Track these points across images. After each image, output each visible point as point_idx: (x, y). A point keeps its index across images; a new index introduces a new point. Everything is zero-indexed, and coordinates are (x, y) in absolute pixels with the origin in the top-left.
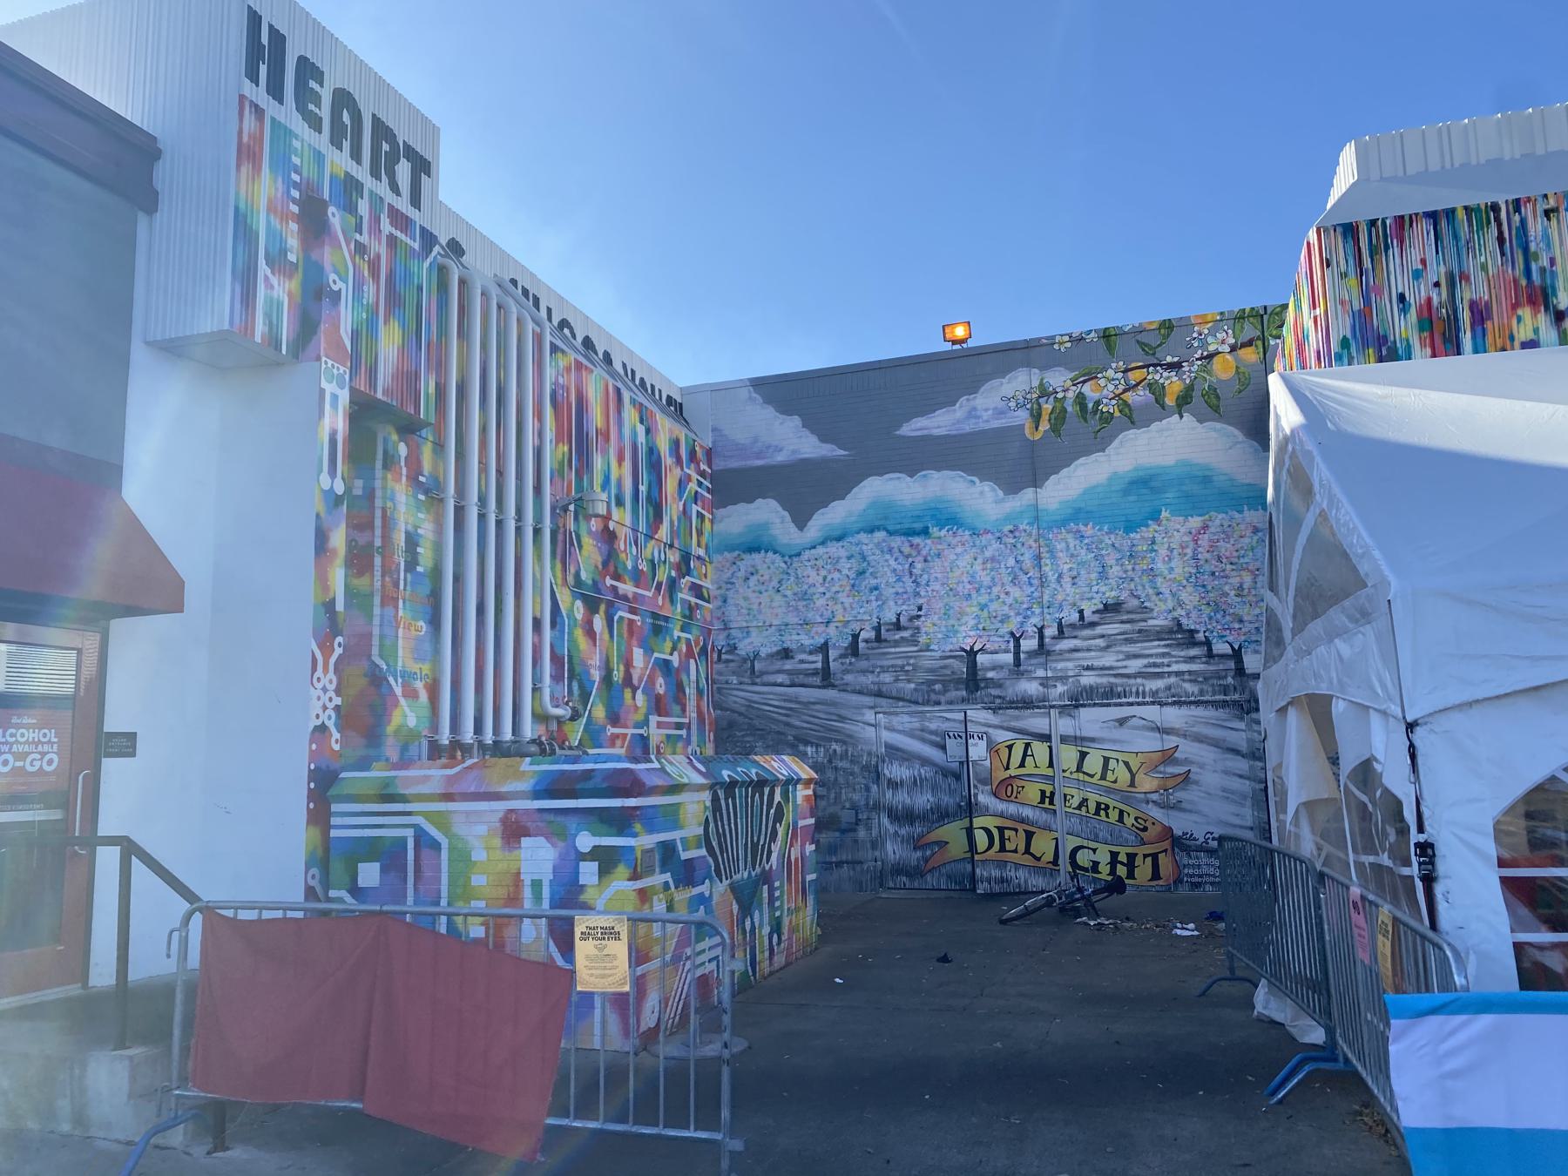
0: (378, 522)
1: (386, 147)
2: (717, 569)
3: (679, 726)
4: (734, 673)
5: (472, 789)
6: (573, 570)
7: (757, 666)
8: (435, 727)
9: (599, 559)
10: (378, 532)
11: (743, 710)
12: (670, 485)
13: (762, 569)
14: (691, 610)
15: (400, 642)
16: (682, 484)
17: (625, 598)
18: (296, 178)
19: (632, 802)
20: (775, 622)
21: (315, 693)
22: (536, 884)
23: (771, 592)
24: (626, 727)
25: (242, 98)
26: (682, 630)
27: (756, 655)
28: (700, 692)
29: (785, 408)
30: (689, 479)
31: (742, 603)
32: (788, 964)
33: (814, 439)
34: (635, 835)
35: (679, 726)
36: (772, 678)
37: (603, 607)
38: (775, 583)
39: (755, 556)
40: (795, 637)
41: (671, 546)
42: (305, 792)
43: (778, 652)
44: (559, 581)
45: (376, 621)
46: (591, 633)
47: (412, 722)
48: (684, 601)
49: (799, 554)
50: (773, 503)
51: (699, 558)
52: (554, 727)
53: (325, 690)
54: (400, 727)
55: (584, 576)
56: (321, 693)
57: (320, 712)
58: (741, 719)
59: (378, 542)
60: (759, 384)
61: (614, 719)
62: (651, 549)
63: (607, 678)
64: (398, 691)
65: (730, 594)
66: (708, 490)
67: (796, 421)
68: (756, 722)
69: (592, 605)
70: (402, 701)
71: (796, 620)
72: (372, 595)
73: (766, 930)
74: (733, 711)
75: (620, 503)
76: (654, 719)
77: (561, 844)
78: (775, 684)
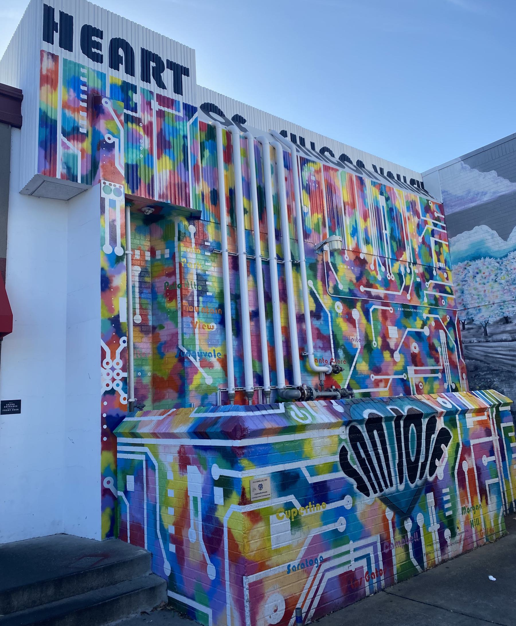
0: (178, 271)
1: (152, 64)
2: (456, 274)
3: (433, 371)
4: (474, 336)
5: (163, 431)
6: (331, 284)
7: (488, 330)
8: (226, 383)
9: (353, 277)
10: (178, 276)
11: (482, 358)
12: (410, 228)
13: (483, 269)
14: (436, 302)
15: (197, 336)
16: (419, 227)
17: (378, 297)
18: (83, 88)
19: (237, 443)
20: (497, 301)
22: (195, 499)
23: (491, 283)
24: (388, 375)
25: (42, 52)
26: (430, 312)
27: (487, 323)
28: (450, 350)
29: (485, 168)
30: (426, 223)
31: (474, 292)
32: (466, 551)
33: (507, 182)
34: (241, 469)
35: (433, 371)
36: (499, 337)
37: (359, 305)
38: (493, 277)
39: (478, 262)
40: (511, 309)
41: (415, 263)
42: (100, 431)
43: (501, 320)
45: (180, 325)
46: (351, 320)
47: (209, 381)
48: (429, 296)
49: (506, 256)
50: (485, 227)
51: (440, 268)
52: (323, 378)
53: (113, 369)
54: (199, 386)
55: (341, 287)
56: (110, 372)
57: (110, 382)
58: (482, 365)
59: (178, 282)
60: (466, 158)
61: (377, 371)
62: (396, 267)
63: (368, 345)
64: (197, 364)
65: (465, 288)
66: (443, 228)
67: (494, 173)
68: (492, 365)
69: (350, 303)
70: (201, 370)
71: (510, 298)
72: (177, 311)
73: (435, 527)
74: (477, 360)
75: (367, 242)
76: (411, 369)
77: (205, 472)
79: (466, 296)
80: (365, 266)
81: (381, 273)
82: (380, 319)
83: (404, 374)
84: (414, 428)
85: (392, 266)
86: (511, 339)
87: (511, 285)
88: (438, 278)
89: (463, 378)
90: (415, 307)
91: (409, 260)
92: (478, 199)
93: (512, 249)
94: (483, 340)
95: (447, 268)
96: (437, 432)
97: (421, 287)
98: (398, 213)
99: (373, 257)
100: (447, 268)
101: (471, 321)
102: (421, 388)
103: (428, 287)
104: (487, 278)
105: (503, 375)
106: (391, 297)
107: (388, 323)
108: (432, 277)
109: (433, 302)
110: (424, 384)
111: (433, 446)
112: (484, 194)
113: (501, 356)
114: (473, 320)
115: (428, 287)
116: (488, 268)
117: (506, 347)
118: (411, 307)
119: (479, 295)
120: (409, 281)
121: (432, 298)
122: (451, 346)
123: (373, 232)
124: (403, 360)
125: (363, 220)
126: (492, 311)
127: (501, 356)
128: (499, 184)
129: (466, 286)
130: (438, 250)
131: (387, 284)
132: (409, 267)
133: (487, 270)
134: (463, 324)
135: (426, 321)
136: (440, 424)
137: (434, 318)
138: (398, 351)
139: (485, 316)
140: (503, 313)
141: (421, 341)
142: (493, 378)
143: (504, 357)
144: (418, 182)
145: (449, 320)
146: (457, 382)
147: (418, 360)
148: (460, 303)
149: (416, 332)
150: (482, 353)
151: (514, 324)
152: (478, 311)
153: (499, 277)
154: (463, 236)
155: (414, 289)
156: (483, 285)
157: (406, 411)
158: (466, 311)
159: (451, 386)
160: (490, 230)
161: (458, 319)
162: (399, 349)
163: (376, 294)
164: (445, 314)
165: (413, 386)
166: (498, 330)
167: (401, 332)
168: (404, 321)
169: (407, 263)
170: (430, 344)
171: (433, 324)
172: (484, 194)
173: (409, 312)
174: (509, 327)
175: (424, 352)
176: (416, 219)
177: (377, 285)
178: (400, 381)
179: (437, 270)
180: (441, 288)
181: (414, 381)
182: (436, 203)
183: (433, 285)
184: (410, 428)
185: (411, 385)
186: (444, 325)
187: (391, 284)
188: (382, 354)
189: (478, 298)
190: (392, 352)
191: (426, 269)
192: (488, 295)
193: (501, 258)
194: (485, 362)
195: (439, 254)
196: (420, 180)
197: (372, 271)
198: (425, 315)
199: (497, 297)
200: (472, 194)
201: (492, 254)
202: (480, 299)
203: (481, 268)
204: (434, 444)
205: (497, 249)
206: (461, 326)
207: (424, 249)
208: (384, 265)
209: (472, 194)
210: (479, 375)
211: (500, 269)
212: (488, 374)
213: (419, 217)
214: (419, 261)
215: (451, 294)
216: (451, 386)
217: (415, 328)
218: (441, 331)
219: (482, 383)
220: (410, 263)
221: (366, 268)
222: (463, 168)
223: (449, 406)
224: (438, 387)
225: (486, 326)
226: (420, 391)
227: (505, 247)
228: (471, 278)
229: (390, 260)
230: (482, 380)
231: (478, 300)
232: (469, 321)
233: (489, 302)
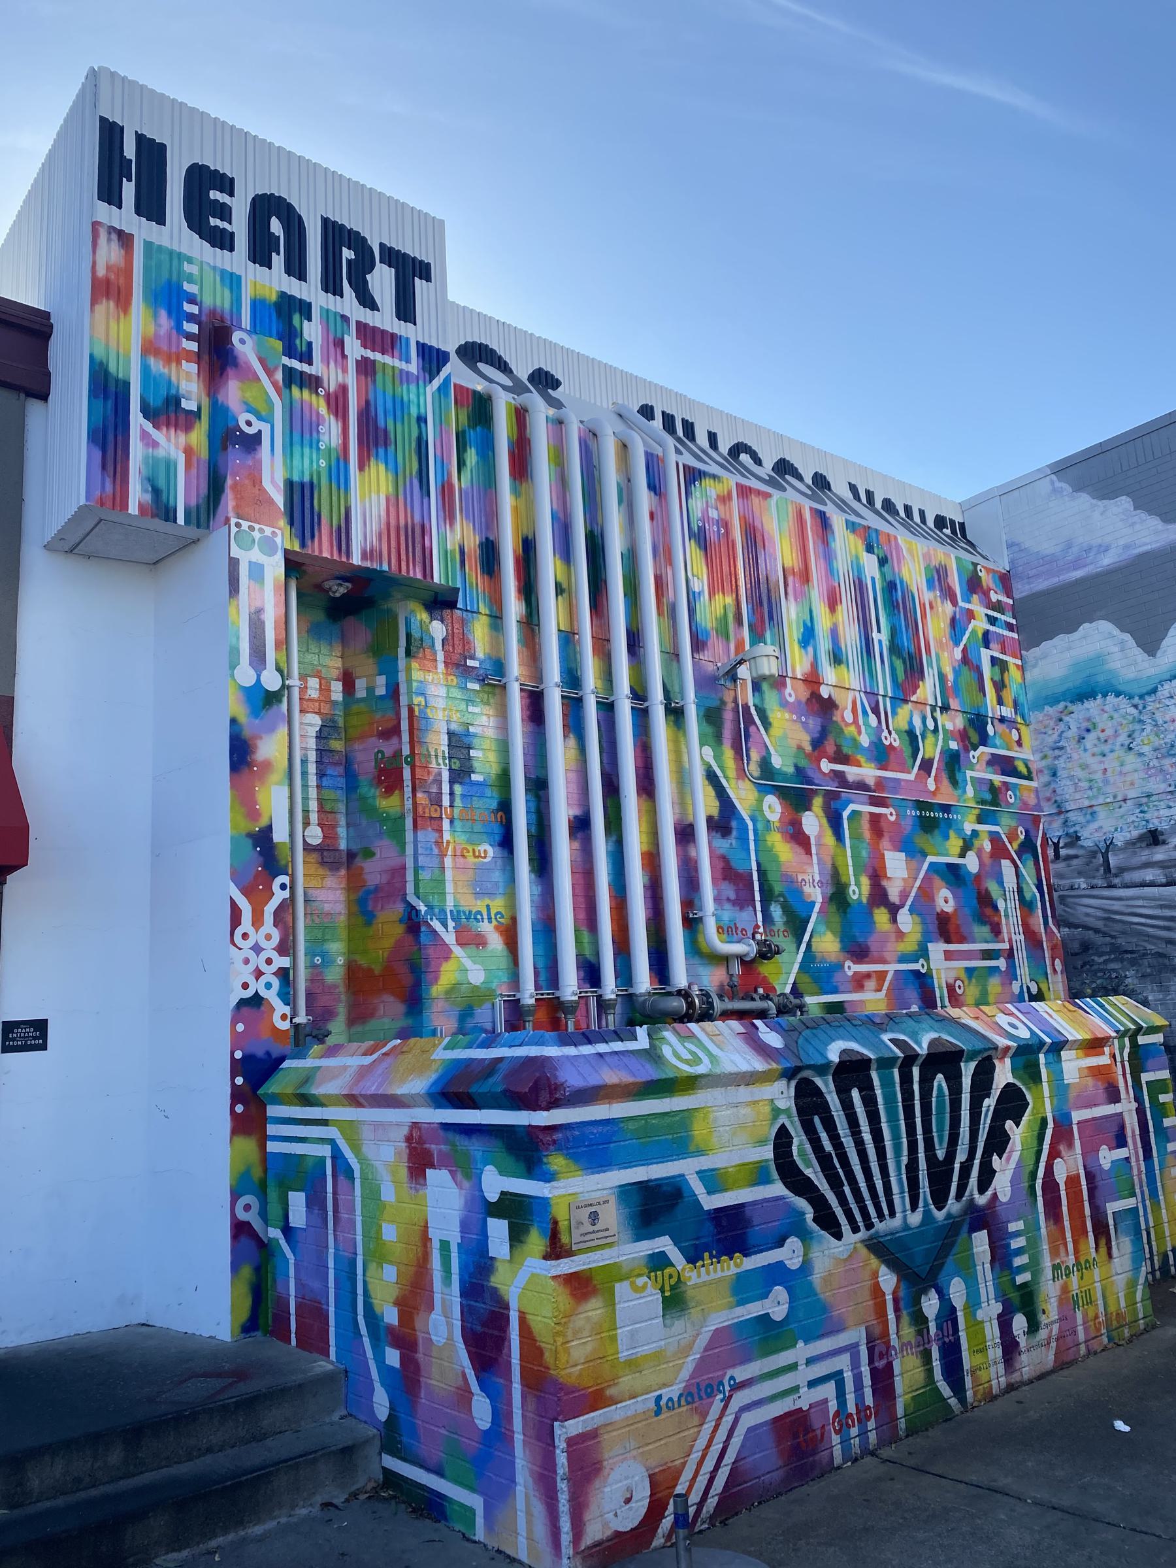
0: (405, 725)
1: (347, 254)
2: (1038, 732)
3: (988, 955)
4: (1080, 874)
5: (372, 1090)
6: (755, 756)
8: (515, 981)
9: (805, 740)
10: (405, 737)
11: (1100, 924)
12: (935, 627)
13: (1102, 721)
14: (993, 796)
15: (449, 874)
16: (956, 626)
17: (861, 786)
18: (190, 308)
19: (541, 1118)
21: (237, 956)
23: (1120, 752)
25: (96, 225)
26: (980, 820)
27: (1110, 845)
28: (1026, 906)
29: (1105, 490)
30: (970, 615)
31: (1079, 773)
32: (1062, 1365)
33: (1154, 522)
34: (549, 1177)
35: (988, 955)
36: (1137, 876)
37: (818, 802)
38: (1123, 738)
39: (1089, 704)
40: (1164, 812)
41: (945, 708)
42: (228, 1090)
43: (1141, 838)
44: (732, 773)
45: (409, 850)
46: (799, 838)
47: (477, 977)
48: (977, 782)
49: (1154, 691)
50: (1105, 626)
51: (1002, 720)
52: (737, 969)
53: (257, 949)
54: (454, 988)
55: (777, 762)
56: (252, 955)
57: (251, 980)
58: (1099, 939)
59: (406, 751)
60: (1062, 469)
62: (903, 716)
63: (838, 896)
64: (450, 938)
65: (1060, 763)
66: (1010, 627)
68: (1121, 941)
69: (797, 799)
70: (457, 951)
71: (1163, 787)
73: (991, 1309)
74: (1086, 928)
75: (837, 659)
76: (937, 949)
77: (466, 1184)
78: (1143, 885)
80: (832, 715)
82: (867, 834)
83: (922, 961)
84: (944, 1085)
85: (894, 713)
86: (1164, 881)
87: (1164, 757)
88: (998, 742)
89: (1055, 971)
90: (946, 808)
91: (931, 701)
93: (1168, 676)
94: (1100, 882)
95: (1019, 720)
99: (851, 695)
100: (1019, 720)
101: (1074, 839)
102: (959, 992)
104: (1110, 742)
105: (1146, 962)
106: (891, 784)
107: (885, 843)
108: (984, 740)
109: (988, 796)
110: (966, 983)
111: (987, 1126)
112: (1104, 549)
113: (1143, 920)
114: (1078, 838)
115: (974, 761)
116: (1112, 718)
120: (931, 749)
121: (985, 788)
122: (1028, 896)
123: (850, 637)
124: (919, 928)
126: (1122, 817)
127: (1143, 920)
128: (1138, 527)
129: (1062, 760)
130: (997, 678)
131: (882, 755)
132: (933, 717)
133: (1110, 724)
134: (1056, 845)
136: (1003, 1075)
137: (990, 832)
138: (907, 907)
140: (1147, 821)
142: (1124, 969)
143: (1149, 921)
144: (952, 522)
145: (1022, 837)
146: (1041, 979)
147: (952, 928)
148: (1049, 799)
149: (949, 865)
150: (1100, 914)
152: (1089, 817)
153: (1138, 740)
155: (943, 766)
156: (1100, 758)
157: (925, 1045)
158: (1062, 816)
159: (1028, 988)
160: (1116, 631)
161: (1044, 834)
162: (909, 903)
163: (857, 778)
164: (1014, 823)
165: (940, 988)
167: (914, 864)
168: (921, 840)
169: (928, 708)
170: (979, 893)
171: (988, 846)
172: (1104, 549)
173: (932, 819)
174: (1160, 854)
175: (967, 911)
176: (948, 608)
177: (859, 757)
178: (911, 977)
179: (996, 722)
180: (1005, 765)
181: (943, 976)
183: (987, 758)
184: (935, 1084)
185: (936, 985)
186: (1012, 848)
187: (892, 757)
188: (871, 914)
189: (1091, 788)
190: (894, 910)
191: (971, 721)
192: (1112, 780)
194: (1105, 934)
195: (999, 686)
196: (958, 519)
197: (847, 725)
198: (969, 827)
199: (1132, 784)
200: (1075, 550)
201: (1121, 688)
203: (1097, 720)
204: (988, 1121)
206: (1051, 852)
207: (967, 675)
209: (1075, 550)
210: (1091, 963)
211: (1140, 721)
213: (954, 603)
214: (954, 704)
215: (1029, 777)
216: (1028, 988)
217: (947, 855)
218: (1006, 863)
219: (1099, 982)
220: (933, 708)
222: (1054, 490)
223: (1024, 1034)
224: (999, 989)
226: (956, 1000)
227: (1152, 671)
229: (888, 699)
230: (1100, 974)
231: (1090, 793)
233: (1115, 797)
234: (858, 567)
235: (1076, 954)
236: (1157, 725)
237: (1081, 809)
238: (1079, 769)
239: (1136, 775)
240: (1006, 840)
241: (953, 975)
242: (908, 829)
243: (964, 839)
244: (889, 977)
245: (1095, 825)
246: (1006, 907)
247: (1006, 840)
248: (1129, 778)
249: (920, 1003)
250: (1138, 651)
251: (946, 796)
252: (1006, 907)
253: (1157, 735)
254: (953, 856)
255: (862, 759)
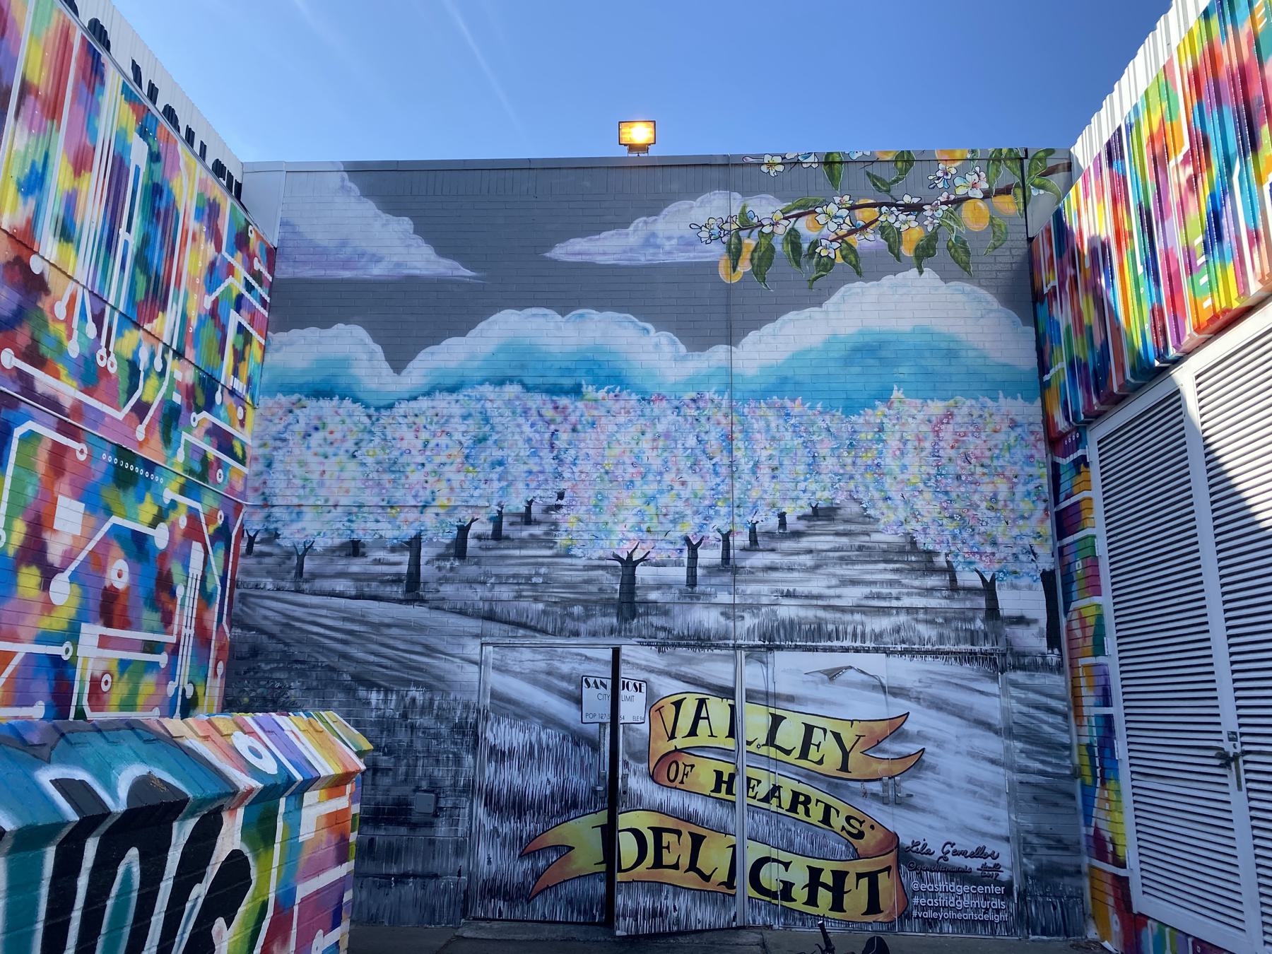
3: (151, 647)
4: (269, 573)
7: (308, 565)
11: (276, 630)
12: (193, 259)
14: (202, 471)
16: (215, 273)
17: (51, 403)
20: (344, 501)
23: (343, 457)
24: (15, 639)
26: (183, 491)
27: (308, 549)
28: (205, 597)
30: (230, 270)
31: (296, 469)
35: (151, 647)
36: (327, 585)
38: (350, 445)
39: (324, 403)
41: (179, 354)
43: (342, 547)
48: (192, 449)
49: (390, 407)
50: (360, 332)
51: (232, 392)
58: (272, 645)
60: (357, 170)
62: (129, 341)
65: (279, 455)
66: (263, 303)
68: (295, 650)
71: (376, 500)
74: (261, 631)
75: (66, 233)
76: (91, 632)
78: (333, 594)
79: (277, 475)
80: (38, 298)
81: (83, 340)
82: (41, 466)
83: (68, 645)
84: (136, 870)
85: (120, 334)
86: (353, 593)
87: (384, 471)
88: (222, 413)
89: (215, 674)
90: (150, 466)
91: (166, 340)
92: (359, 265)
93: (407, 396)
94: (288, 585)
95: (248, 399)
96: (212, 871)
97: (177, 419)
98: (172, 209)
99: (71, 286)
100: (248, 399)
101: (272, 536)
102: (105, 688)
103: (194, 424)
104: (336, 445)
105: (314, 674)
106: (93, 416)
107: (63, 485)
108: (209, 406)
109: (197, 467)
110: (116, 677)
111: (187, 936)
112: (376, 259)
113: (322, 631)
114: (277, 536)
115: (194, 424)
116: (343, 422)
117: (340, 611)
118: (139, 461)
119: (306, 480)
120: (152, 392)
121: (198, 457)
122: (210, 587)
123: (91, 215)
124: (76, 602)
125: (70, 169)
126: (328, 522)
127: (322, 631)
128: (413, 250)
129: (281, 452)
130: (239, 347)
131: (90, 376)
132: (163, 358)
133: (340, 427)
134: (251, 540)
135: (167, 510)
136: (230, 838)
137: (190, 508)
138: (68, 573)
139: (309, 532)
140: (352, 531)
141: (139, 561)
142: (290, 679)
143: (328, 632)
144: (230, 176)
145: (220, 522)
146: (199, 682)
147: (117, 609)
148: (256, 490)
149: (135, 534)
150: (279, 618)
151: (370, 559)
152: (294, 515)
153: (364, 450)
154: (305, 338)
155: (159, 417)
156: (321, 459)
157: (123, 792)
158: (266, 510)
159: (184, 691)
160: (368, 339)
161: (242, 525)
162: (72, 567)
163: (50, 392)
164: (216, 505)
165: (82, 681)
166: (330, 569)
167: (93, 521)
168: (110, 494)
169: (161, 346)
170: (160, 573)
171: (183, 522)
172: (376, 259)
173: (129, 473)
174: (356, 566)
175: (141, 591)
176: (211, 248)
177: (60, 367)
178: (47, 662)
179: (226, 391)
180: (224, 441)
181: (90, 665)
182: (263, 240)
183: (208, 426)
184: (121, 870)
185: (78, 677)
186: (208, 531)
187: (103, 383)
188: (15, 572)
189: (304, 487)
190: (49, 573)
191: (201, 380)
192: (328, 483)
193: (378, 409)
194: (280, 641)
195: (239, 356)
196: (237, 177)
197: (56, 320)
198: (169, 494)
199: (347, 491)
200: (349, 250)
201: (361, 396)
202: (307, 490)
203: (328, 420)
204: (190, 927)
205: (374, 387)
206: (243, 546)
207: (210, 330)
208: (98, 320)
209: (349, 250)
210: (257, 670)
211: (371, 432)
212: (279, 669)
213: (218, 248)
214: (190, 353)
215: (242, 462)
216: (184, 691)
217: (135, 520)
218: (197, 547)
219: (259, 691)
220: (167, 348)
221: (40, 305)
222: (343, 187)
223: (270, 767)
224: (152, 689)
225: (304, 555)
226: (98, 698)
227: (393, 388)
228: (298, 438)
229: (117, 315)
230: (262, 683)
231: (301, 492)
232: (266, 536)
233: (326, 501)
234: (121, 137)
235: (242, 658)
236: (385, 440)
237: (288, 506)
238: (296, 465)
239: (353, 483)
240: (203, 520)
241: (102, 666)
242: (99, 476)
243: (160, 508)
244: (16, 661)
245: (299, 525)
246: (185, 596)
247: (203, 520)
248: (346, 485)
249: (49, 699)
250: (386, 365)
251: (153, 452)
252: (185, 596)
253: (383, 449)
254: (142, 523)
255: (63, 372)
